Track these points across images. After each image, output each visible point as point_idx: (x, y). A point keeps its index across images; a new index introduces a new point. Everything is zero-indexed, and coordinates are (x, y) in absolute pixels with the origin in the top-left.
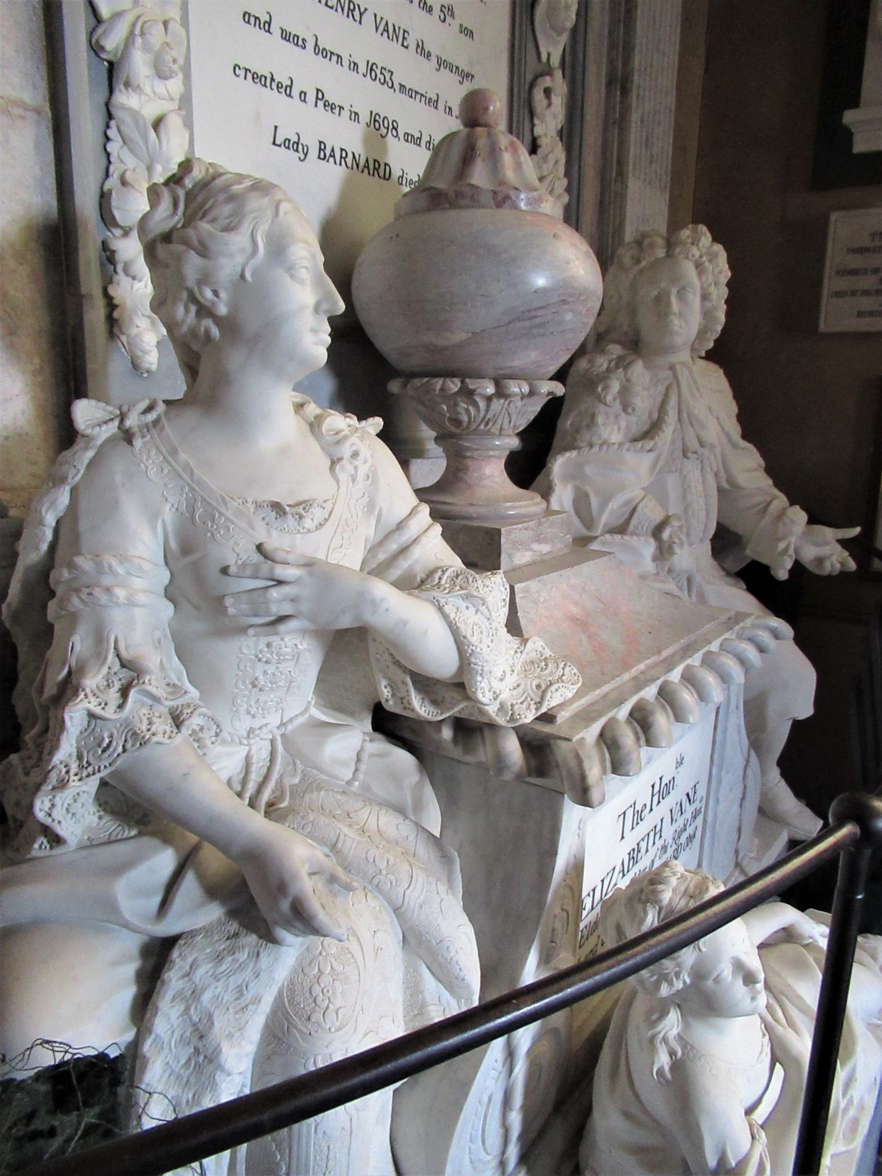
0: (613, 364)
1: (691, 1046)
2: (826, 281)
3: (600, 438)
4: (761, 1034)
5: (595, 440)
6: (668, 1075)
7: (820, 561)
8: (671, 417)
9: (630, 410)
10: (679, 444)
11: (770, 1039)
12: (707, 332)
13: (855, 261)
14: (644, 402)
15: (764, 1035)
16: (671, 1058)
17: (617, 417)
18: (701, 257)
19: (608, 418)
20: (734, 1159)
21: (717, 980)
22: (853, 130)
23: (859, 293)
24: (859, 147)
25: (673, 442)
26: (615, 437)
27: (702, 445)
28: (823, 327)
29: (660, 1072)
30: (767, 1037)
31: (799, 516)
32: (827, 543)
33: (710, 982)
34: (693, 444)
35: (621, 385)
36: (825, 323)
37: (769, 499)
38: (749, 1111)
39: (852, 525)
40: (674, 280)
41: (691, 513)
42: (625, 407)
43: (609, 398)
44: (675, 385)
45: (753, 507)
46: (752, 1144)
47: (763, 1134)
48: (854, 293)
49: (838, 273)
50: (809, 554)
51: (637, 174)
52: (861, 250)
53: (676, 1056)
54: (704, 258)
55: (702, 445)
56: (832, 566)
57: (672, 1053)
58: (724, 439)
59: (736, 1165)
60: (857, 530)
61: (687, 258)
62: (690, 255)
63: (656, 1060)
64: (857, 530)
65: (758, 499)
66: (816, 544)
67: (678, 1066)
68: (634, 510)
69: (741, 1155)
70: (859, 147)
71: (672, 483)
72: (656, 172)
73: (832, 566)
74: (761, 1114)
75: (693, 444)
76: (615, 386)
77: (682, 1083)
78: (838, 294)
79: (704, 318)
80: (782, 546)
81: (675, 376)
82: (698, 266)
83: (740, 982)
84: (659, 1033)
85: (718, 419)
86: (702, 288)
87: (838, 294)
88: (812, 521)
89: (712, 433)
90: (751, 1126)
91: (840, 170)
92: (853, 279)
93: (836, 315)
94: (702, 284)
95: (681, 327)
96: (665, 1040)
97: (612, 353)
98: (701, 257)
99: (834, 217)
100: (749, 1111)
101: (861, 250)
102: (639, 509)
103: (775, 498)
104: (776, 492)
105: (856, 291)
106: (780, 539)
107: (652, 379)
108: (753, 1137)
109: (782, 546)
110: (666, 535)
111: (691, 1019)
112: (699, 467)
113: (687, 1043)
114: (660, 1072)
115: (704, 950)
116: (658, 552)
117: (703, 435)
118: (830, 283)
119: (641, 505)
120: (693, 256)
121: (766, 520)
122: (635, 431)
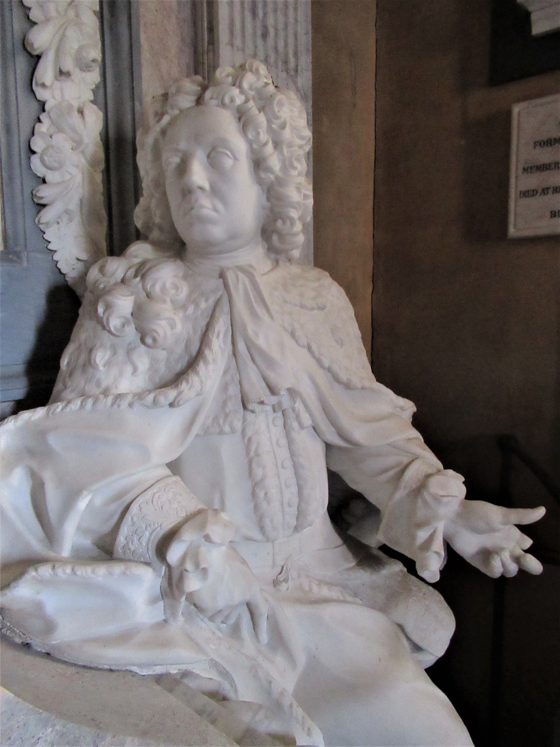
0: (132, 272)
2: (513, 181)
3: (98, 385)
5: (92, 389)
7: (487, 554)
8: (218, 348)
9: (149, 341)
10: (234, 390)
12: (275, 221)
13: (545, 156)
14: (173, 327)
17: (129, 351)
18: (247, 101)
19: (114, 353)
22: (530, 9)
23: (551, 191)
24: (539, 27)
25: (224, 388)
26: (128, 383)
27: (273, 390)
28: (512, 231)
31: (454, 484)
34: (257, 389)
35: (135, 302)
36: (515, 225)
37: (406, 460)
39: (533, 505)
40: (197, 138)
41: (261, 494)
42: (144, 335)
43: (114, 323)
44: (225, 298)
45: (385, 471)
48: (545, 191)
49: (525, 170)
50: (468, 546)
51: (238, 42)
52: (549, 143)
54: (251, 104)
55: (273, 390)
58: (322, 377)
60: (540, 512)
61: (223, 105)
62: (227, 100)
64: (540, 512)
65: (391, 460)
66: (476, 530)
68: (127, 508)
70: (539, 27)
71: (229, 449)
72: (276, 49)
75: (257, 389)
76: (124, 304)
78: (526, 194)
79: (268, 199)
80: (422, 535)
81: (226, 286)
82: (242, 116)
85: (309, 349)
86: (252, 151)
87: (526, 194)
88: (474, 492)
89: (294, 369)
91: (519, 55)
92: (544, 175)
93: (525, 218)
94: (250, 143)
95: (215, 210)
97: (136, 257)
98: (247, 101)
99: (516, 109)
101: (549, 143)
102: (134, 508)
105: (548, 189)
106: (420, 525)
107: (191, 292)
109: (422, 535)
110: (175, 554)
112: (280, 422)
116: (166, 584)
117: (271, 375)
118: (518, 182)
119: (140, 500)
120: (232, 100)
121: (400, 494)
122: (164, 372)
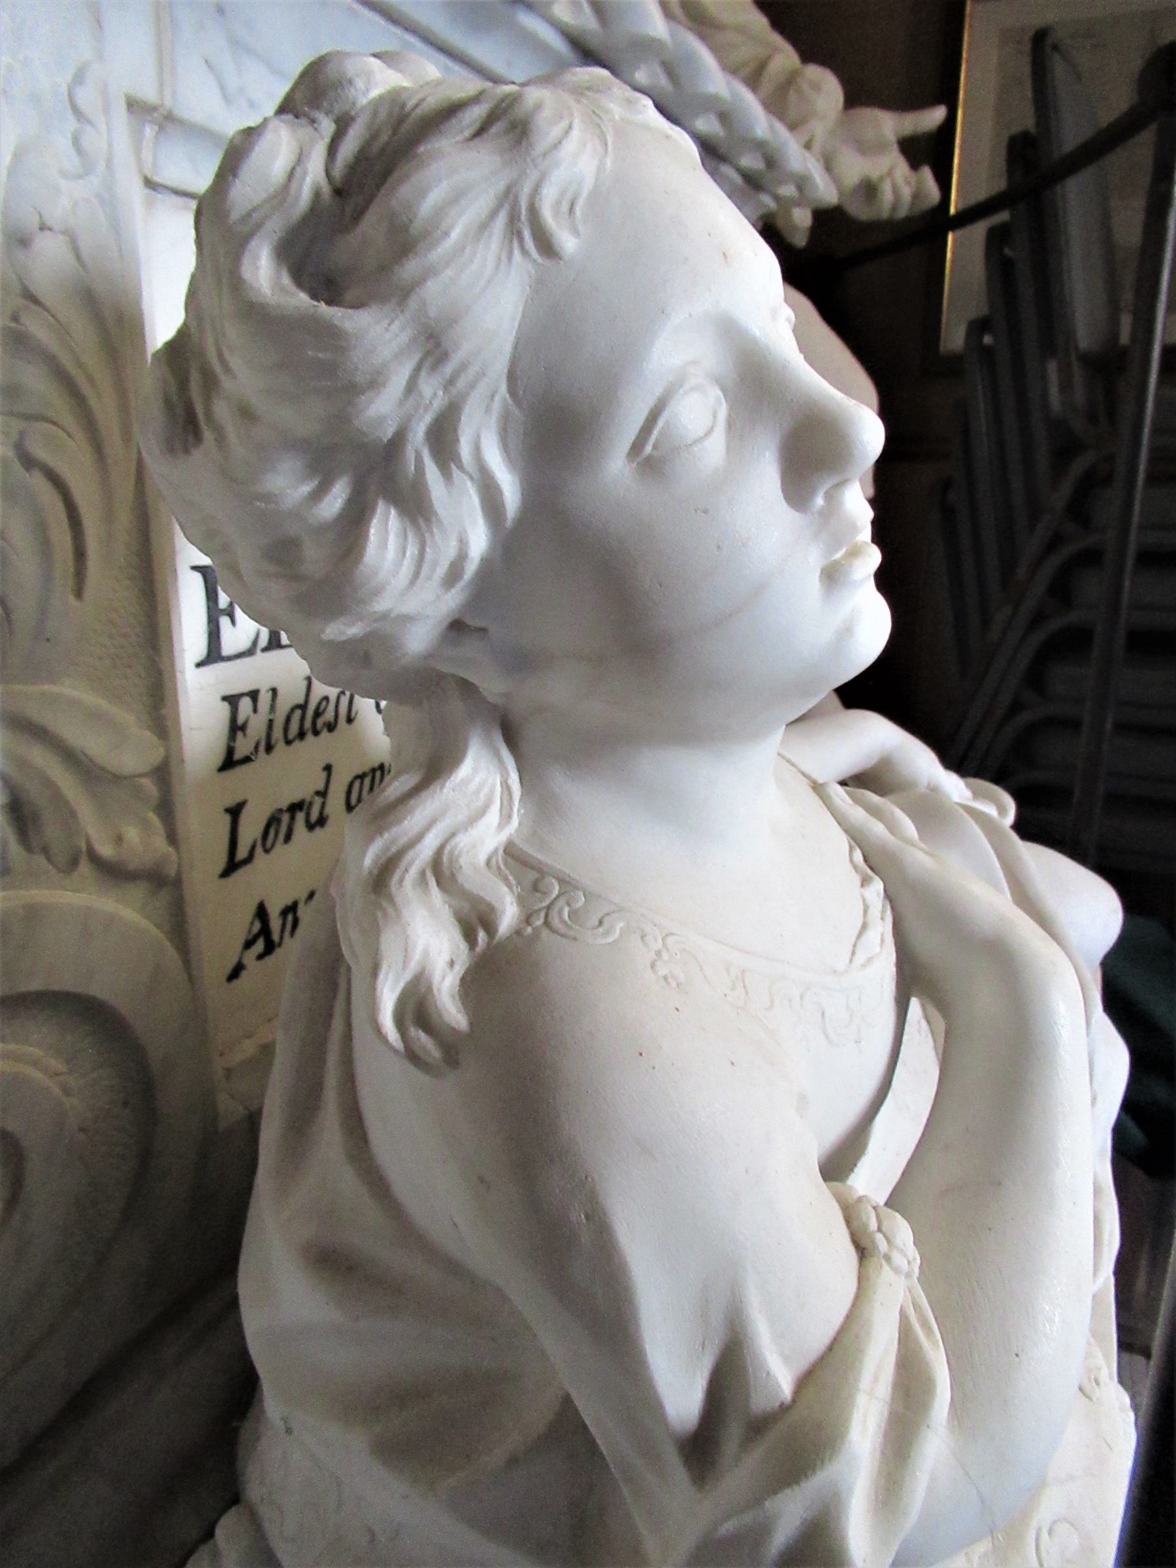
1: (562, 881)
4: (857, 880)
6: (451, 1009)
11: (888, 895)
15: (865, 881)
16: (469, 936)
20: (786, 1359)
21: (653, 459)
29: (416, 1008)
30: (878, 885)
32: (879, 148)
33: (616, 466)
38: (837, 1165)
46: (863, 1280)
47: (903, 1231)
53: (490, 928)
56: (896, 190)
57: (474, 920)
59: (804, 1382)
63: (389, 945)
67: (501, 970)
69: (818, 1338)
73: (896, 190)
74: (874, 1177)
77: (516, 1048)
83: (766, 474)
84: (418, 838)
88: (853, 100)
90: (850, 1212)
96: (441, 871)
100: (837, 1165)
103: (776, 50)
104: (777, 39)
108: (863, 1249)
111: (561, 782)
113: (541, 871)
114: (416, 1008)
115: (568, 243)
